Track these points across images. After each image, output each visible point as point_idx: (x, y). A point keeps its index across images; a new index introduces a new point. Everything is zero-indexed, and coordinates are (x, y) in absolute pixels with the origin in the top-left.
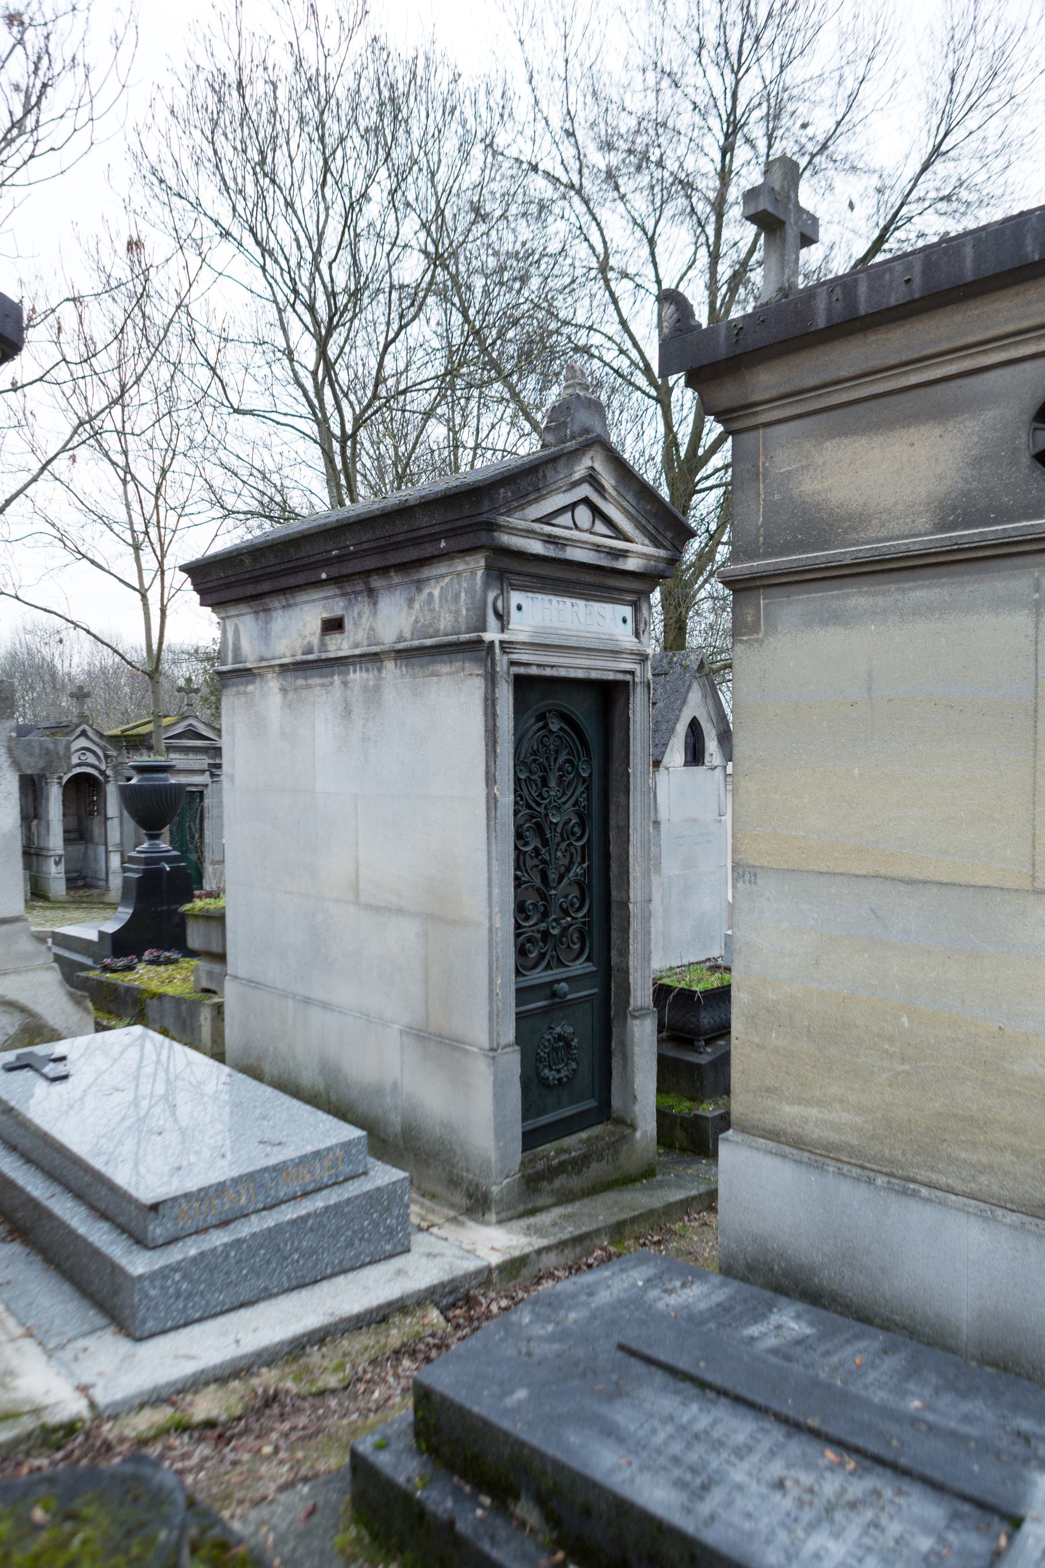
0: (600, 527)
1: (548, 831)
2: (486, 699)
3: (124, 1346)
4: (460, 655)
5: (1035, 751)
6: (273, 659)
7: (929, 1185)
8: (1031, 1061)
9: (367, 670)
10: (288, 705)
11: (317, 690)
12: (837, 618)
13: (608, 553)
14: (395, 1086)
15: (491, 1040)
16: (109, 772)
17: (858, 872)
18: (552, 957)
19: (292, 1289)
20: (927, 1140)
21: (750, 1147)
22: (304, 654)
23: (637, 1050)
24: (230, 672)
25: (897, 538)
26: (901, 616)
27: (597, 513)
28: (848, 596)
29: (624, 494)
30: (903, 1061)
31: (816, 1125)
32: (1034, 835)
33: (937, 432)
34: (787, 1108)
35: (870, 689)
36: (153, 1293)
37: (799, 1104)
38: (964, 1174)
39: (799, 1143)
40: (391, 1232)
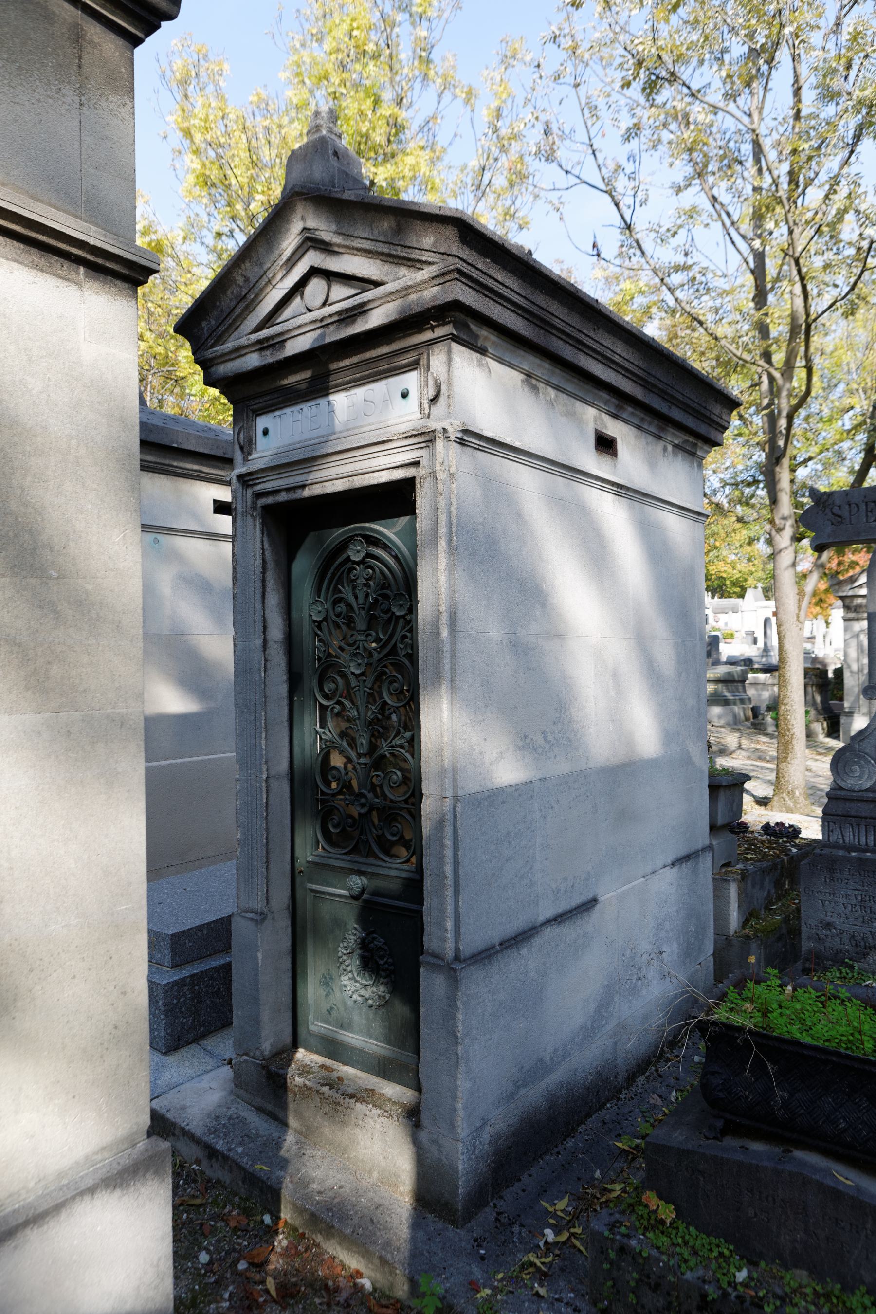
27: (330, 276)
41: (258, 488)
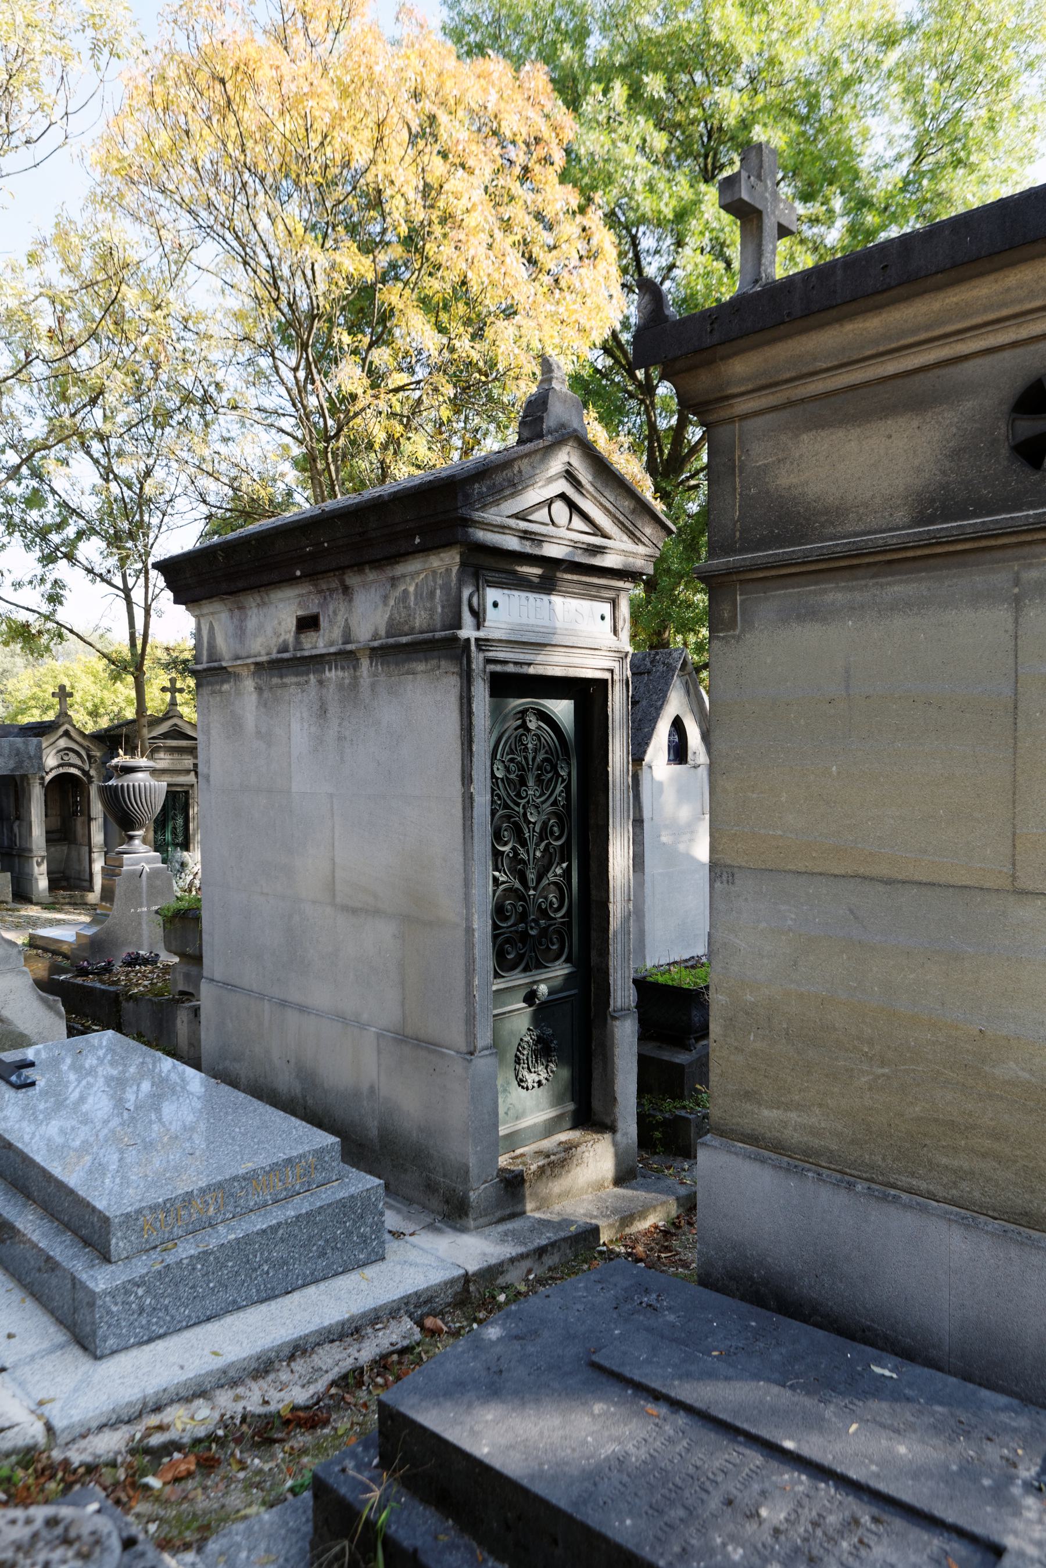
0: (578, 523)
1: (526, 831)
2: (461, 698)
3: (85, 1365)
4: (436, 653)
5: (1015, 747)
6: (248, 657)
7: (909, 1191)
8: (1012, 1065)
9: (343, 668)
10: (263, 704)
11: (293, 689)
12: (812, 614)
13: (586, 550)
14: (372, 1089)
15: (468, 1043)
16: (92, 773)
17: (836, 872)
18: (531, 957)
19: (262, 1301)
20: (908, 1145)
21: (729, 1152)
22: (279, 652)
23: (617, 1051)
24: (205, 670)
25: (875, 532)
26: (879, 611)
27: (573, 506)
28: (825, 591)
29: (602, 489)
30: (883, 1065)
31: (795, 1130)
32: (1014, 834)
33: (915, 423)
34: (766, 1112)
35: (847, 687)
36: (114, 1309)
37: (778, 1108)
38: (945, 1180)
39: (778, 1147)
40: (364, 1239)
41: (490, 654)
